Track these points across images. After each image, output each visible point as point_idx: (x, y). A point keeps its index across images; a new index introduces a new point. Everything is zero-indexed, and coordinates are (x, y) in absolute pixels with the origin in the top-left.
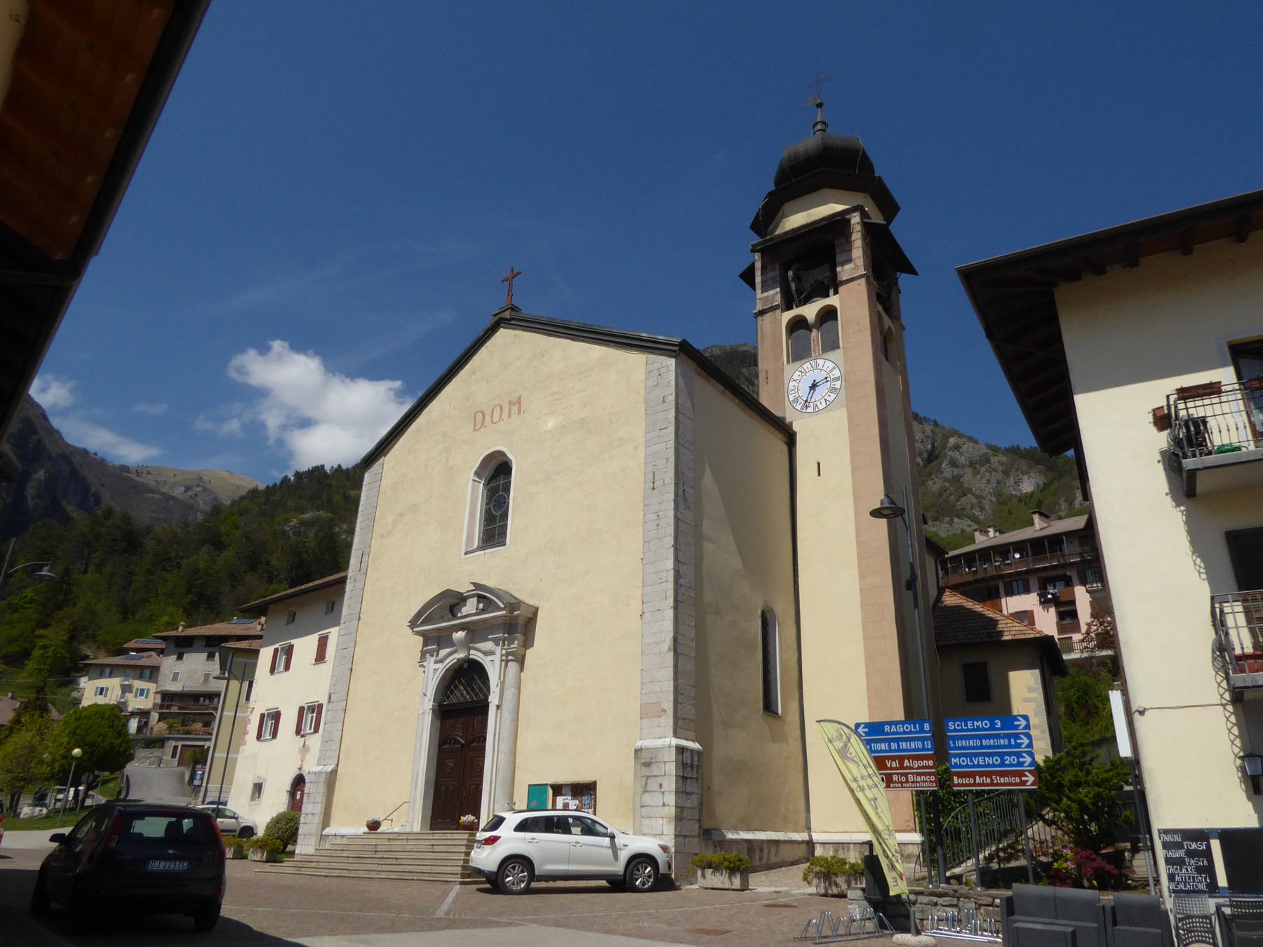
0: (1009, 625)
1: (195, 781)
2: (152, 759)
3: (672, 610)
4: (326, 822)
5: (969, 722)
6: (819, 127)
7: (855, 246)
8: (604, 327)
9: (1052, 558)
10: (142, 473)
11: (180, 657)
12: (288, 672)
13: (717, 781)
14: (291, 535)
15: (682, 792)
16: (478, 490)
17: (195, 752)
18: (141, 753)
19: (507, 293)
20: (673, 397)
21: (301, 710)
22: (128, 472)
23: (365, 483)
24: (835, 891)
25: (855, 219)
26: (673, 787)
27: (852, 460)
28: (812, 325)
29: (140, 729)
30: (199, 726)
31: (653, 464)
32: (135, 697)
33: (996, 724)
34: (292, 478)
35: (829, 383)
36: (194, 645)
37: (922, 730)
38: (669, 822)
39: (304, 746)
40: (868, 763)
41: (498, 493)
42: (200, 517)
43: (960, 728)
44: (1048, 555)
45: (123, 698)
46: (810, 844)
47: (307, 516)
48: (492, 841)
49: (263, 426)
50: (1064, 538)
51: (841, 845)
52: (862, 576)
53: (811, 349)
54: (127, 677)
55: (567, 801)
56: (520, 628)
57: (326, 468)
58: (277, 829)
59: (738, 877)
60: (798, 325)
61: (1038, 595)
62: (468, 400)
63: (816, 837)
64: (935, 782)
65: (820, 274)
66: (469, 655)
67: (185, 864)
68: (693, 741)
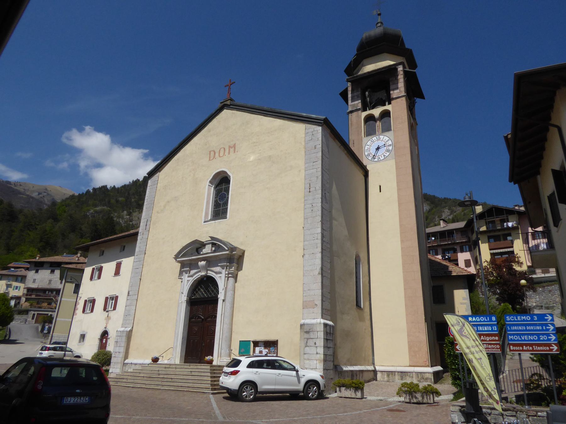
0: (454, 268)
1: (44, 331)
2: (22, 320)
4: (126, 357)
5: (518, 317)
6: (379, 25)
7: (400, 82)
9: (449, 240)
10: (17, 185)
11: (37, 272)
12: (100, 280)
13: (339, 340)
14: (90, 217)
15: (326, 347)
16: (211, 191)
17: (44, 317)
18: (16, 317)
19: (228, 92)
20: (320, 146)
21: (107, 299)
22: (10, 184)
23: (148, 185)
24: (415, 401)
25: (400, 68)
26: (322, 344)
27: (398, 186)
28: (377, 119)
29: (15, 305)
30: (45, 304)
31: (309, 179)
32: (13, 290)
33: (534, 318)
34: (91, 191)
35: (386, 147)
36: (44, 266)
39: (108, 316)
40: (476, 338)
41: (221, 192)
42: (46, 207)
43: (513, 320)
44: (447, 238)
45: (7, 290)
46: (375, 372)
47: (98, 208)
48: (235, 373)
49: (78, 166)
50: (455, 231)
51: (391, 373)
52: (402, 241)
54: (9, 280)
55: (262, 350)
56: (235, 261)
57: (108, 187)
58: (98, 359)
59: (360, 392)
60: (370, 119)
61: (442, 256)
62: (206, 145)
63: (378, 368)
64: (500, 348)
65: (382, 95)
66: (207, 273)
67: (87, 399)
68: (329, 320)
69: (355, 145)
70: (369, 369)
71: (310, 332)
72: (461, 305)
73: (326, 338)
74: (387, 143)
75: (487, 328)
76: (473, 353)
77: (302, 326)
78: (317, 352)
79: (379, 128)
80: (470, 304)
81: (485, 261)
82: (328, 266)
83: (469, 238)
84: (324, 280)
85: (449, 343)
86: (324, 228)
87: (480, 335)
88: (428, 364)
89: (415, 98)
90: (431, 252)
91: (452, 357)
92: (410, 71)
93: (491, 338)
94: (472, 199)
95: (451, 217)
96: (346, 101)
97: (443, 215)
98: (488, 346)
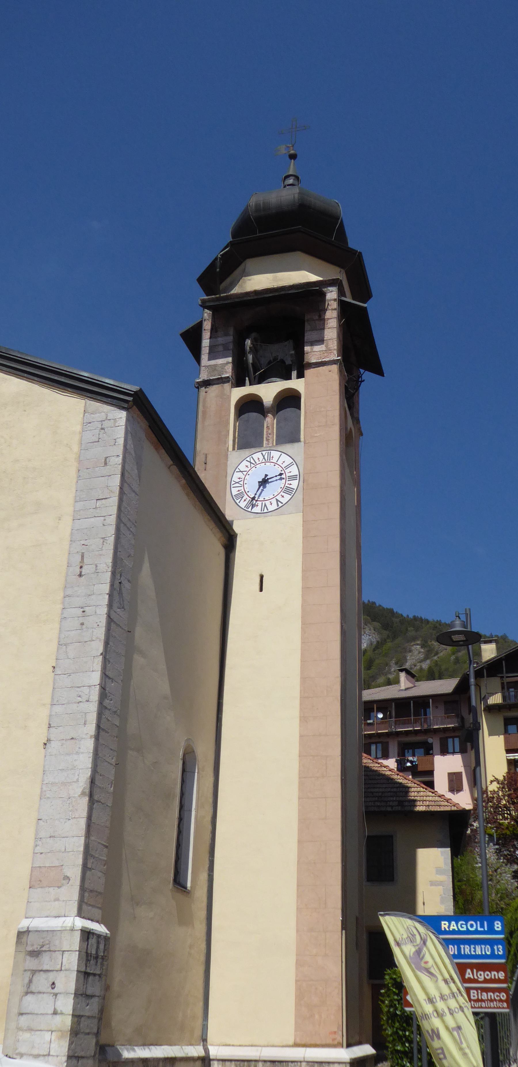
0: (422, 794)
3: (93, 739)
6: (291, 181)
8: (27, 355)
9: (416, 721)
20: (120, 460)
26: (72, 987)
28: (268, 408)
31: (83, 542)
35: (284, 481)
37: (491, 930)
38: (61, 1037)
44: (412, 718)
51: (246, 1063)
52: (304, 719)
53: (263, 438)
61: (397, 761)
63: (214, 1052)
64: (506, 1001)
68: (98, 922)
69: (208, 466)
70: (190, 1055)
71: (43, 952)
72: (433, 887)
73: (83, 969)
74: (287, 471)
75: (481, 948)
76: (440, 1015)
77: (22, 935)
78: (55, 1009)
79: (270, 431)
80: (451, 886)
81: (493, 779)
82: (111, 773)
83: (463, 719)
84: (94, 811)
85: (393, 986)
86: (109, 673)
87: (461, 969)
88: (339, 1038)
89: (362, 371)
90: (373, 747)
91: (398, 1021)
92: (354, 304)
93: (488, 975)
94: (469, 630)
95: (425, 665)
96: (196, 353)
97: (408, 658)
98: (481, 995)
